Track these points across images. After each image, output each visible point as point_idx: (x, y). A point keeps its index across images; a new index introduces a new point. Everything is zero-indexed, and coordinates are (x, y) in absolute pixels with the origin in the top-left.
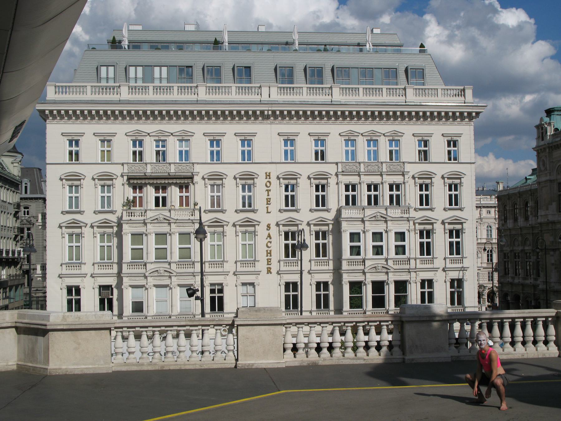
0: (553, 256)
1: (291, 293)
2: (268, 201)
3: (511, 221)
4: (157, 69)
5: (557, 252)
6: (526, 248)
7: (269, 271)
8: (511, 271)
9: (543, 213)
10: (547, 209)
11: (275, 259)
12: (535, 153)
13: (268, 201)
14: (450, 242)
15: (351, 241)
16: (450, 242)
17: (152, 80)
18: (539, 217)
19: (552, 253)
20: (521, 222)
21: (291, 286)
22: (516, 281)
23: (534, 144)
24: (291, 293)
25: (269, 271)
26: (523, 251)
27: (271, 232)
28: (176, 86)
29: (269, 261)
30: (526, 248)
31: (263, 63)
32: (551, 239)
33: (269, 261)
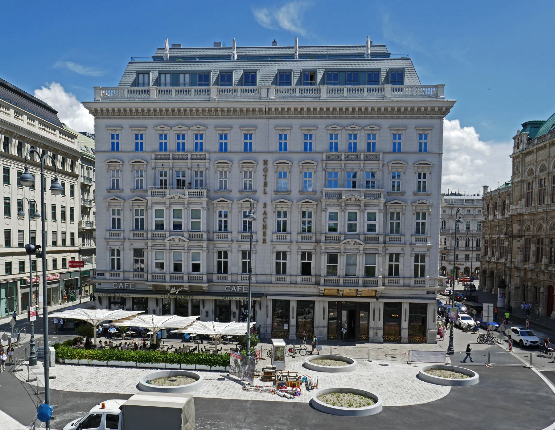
0: (519, 241)
1: (223, 260)
2: (265, 184)
3: (492, 216)
4: (182, 76)
5: (523, 239)
6: (502, 236)
7: (264, 241)
8: (489, 253)
9: (514, 208)
10: (517, 204)
11: (269, 232)
12: (512, 159)
13: (265, 184)
14: (136, 219)
15: (374, 225)
16: (136, 219)
17: (178, 85)
18: (511, 211)
19: (518, 239)
20: (499, 216)
21: (281, 255)
22: (493, 260)
23: (511, 152)
24: (223, 260)
25: (264, 241)
26: (499, 238)
27: (266, 209)
28: (193, 88)
29: (264, 234)
30: (502, 236)
31: (266, 72)
32: (519, 228)
33: (264, 234)
